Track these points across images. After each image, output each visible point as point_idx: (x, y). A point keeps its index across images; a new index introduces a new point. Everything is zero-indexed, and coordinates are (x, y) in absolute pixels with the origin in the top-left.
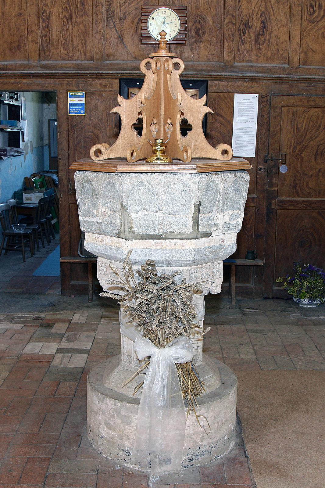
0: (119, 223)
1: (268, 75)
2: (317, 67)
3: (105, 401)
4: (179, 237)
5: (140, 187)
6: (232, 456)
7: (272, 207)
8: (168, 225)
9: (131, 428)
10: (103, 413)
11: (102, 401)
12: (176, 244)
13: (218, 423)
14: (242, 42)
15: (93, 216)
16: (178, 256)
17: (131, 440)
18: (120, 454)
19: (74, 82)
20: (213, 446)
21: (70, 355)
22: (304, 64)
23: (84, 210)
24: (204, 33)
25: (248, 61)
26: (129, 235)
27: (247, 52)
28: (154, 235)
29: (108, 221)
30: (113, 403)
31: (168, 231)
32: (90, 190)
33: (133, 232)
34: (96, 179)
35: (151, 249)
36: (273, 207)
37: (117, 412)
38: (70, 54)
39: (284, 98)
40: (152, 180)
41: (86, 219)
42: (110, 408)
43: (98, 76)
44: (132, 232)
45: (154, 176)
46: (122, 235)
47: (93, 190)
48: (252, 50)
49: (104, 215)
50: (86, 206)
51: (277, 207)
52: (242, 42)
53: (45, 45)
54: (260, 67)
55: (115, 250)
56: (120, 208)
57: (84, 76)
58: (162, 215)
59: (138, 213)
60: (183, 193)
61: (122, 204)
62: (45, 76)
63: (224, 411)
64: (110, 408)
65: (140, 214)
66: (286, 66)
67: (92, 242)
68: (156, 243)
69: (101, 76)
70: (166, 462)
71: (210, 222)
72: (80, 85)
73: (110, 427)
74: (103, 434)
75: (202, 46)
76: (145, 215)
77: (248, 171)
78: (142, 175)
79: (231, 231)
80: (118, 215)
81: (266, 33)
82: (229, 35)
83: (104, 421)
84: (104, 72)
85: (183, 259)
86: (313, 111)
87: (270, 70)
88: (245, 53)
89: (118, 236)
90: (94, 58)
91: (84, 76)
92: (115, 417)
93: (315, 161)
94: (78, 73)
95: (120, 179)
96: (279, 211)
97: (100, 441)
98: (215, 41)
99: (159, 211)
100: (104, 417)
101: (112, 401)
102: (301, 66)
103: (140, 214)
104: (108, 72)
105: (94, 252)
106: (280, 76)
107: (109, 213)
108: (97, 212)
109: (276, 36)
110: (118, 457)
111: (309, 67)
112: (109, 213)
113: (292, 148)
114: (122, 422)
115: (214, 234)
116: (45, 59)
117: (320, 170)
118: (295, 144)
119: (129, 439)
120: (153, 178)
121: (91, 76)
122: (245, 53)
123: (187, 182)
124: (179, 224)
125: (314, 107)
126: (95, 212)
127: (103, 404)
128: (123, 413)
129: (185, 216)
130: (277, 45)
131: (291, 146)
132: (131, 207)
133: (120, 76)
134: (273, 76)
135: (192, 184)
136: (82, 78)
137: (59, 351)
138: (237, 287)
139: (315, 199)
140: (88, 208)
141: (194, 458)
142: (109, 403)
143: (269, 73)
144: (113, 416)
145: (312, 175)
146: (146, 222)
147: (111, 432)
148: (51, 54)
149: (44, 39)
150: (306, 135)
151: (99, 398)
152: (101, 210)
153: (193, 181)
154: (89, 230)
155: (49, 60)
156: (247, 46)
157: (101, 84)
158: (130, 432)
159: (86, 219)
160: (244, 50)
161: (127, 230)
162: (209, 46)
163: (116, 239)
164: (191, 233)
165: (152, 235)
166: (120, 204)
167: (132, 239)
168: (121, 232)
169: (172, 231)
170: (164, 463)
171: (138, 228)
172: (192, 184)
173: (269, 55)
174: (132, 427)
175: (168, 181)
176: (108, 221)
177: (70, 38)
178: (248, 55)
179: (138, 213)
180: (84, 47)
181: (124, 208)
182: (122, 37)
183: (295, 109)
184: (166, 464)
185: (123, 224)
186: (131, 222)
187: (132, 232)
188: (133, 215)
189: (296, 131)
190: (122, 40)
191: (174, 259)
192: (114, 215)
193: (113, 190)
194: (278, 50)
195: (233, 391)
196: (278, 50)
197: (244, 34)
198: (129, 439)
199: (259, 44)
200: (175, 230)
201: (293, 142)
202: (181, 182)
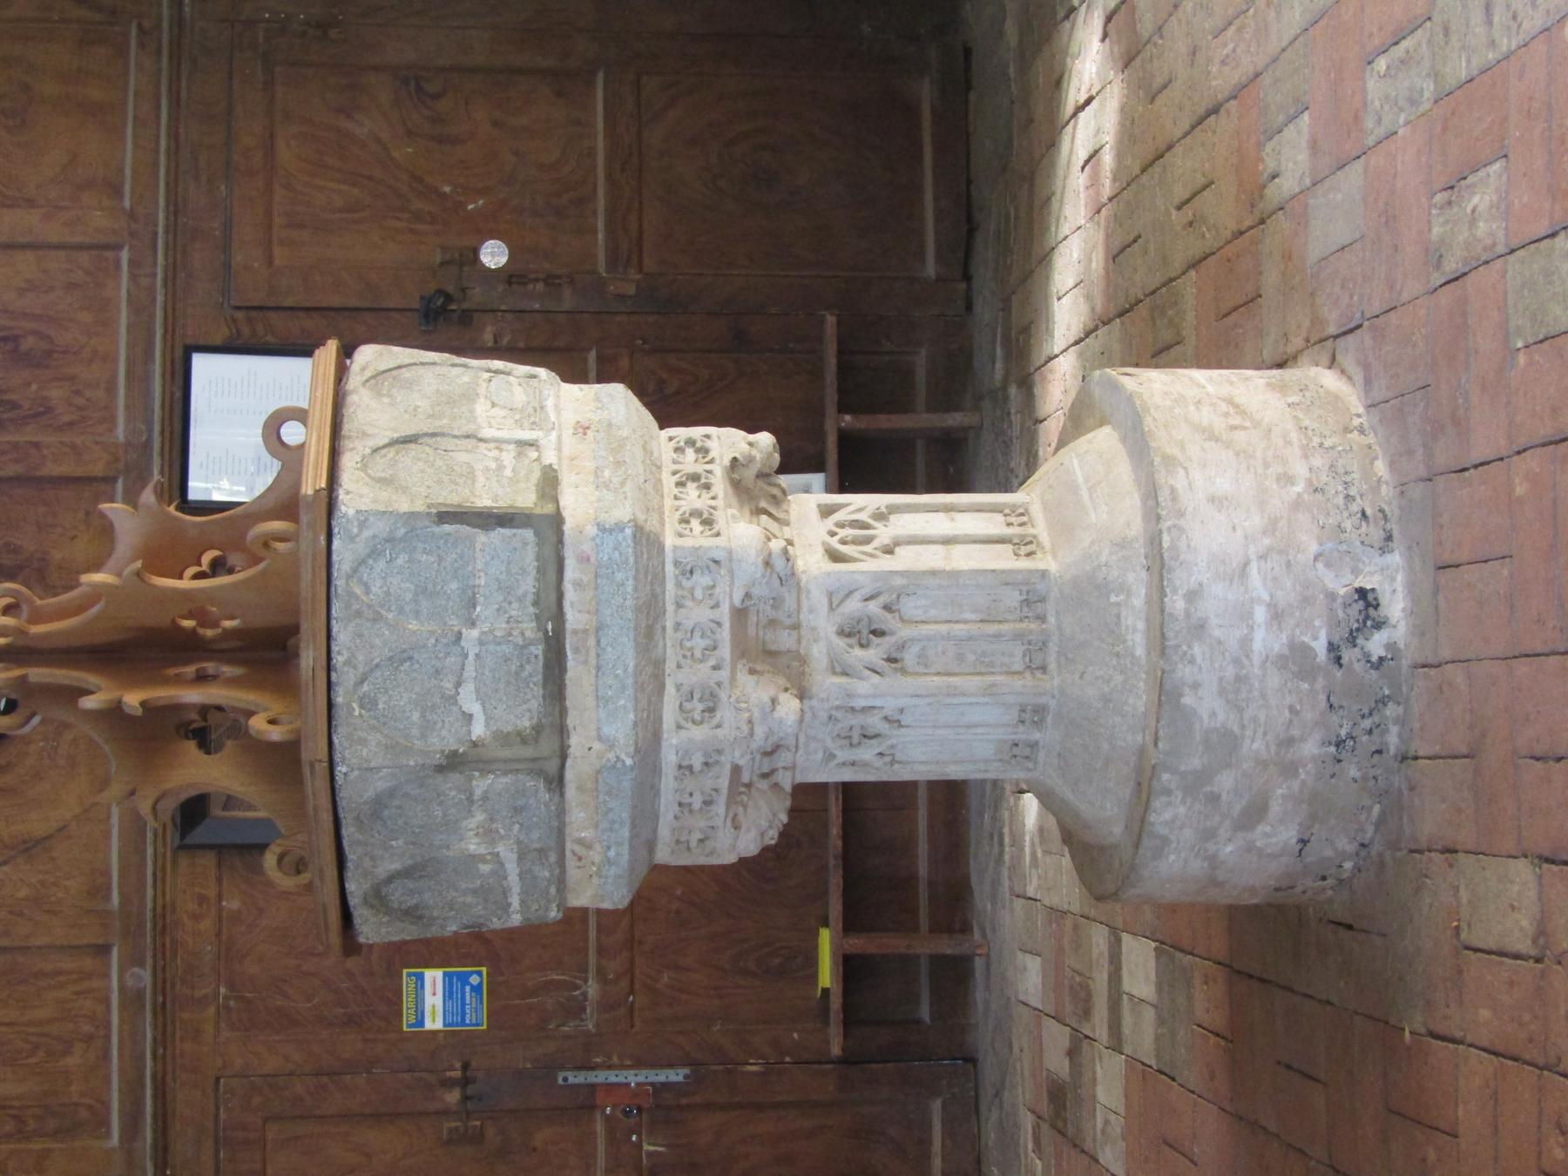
0: (505, 780)
1: (159, 314)
2: (130, 146)
3: (1163, 831)
4: (552, 576)
5: (381, 706)
6: (1359, 377)
7: (632, 290)
8: (514, 613)
9: (1248, 733)
10: (1209, 835)
11: (1165, 840)
12: (578, 585)
13: (1233, 428)
14: (42, 414)
15: (500, 873)
16: (619, 576)
17: (1295, 732)
18: (1353, 772)
19: (186, 1016)
20: (1316, 440)
21: (1125, 997)
22: (117, 192)
23: (485, 908)
24: (16, 550)
25: (111, 388)
26: (547, 746)
27: (78, 393)
28: (545, 658)
29: (507, 822)
30: (1164, 799)
31: (532, 610)
32: (410, 884)
33: (538, 729)
34: (367, 863)
35: (598, 668)
36: (631, 290)
37: (1195, 784)
38: (87, 1028)
39: (238, 259)
40: (355, 667)
41: (515, 901)
42: (1182, 810)
43: (164, 927)
44: (538, 733)
45: (339, 660)
46: (552, 767)
47: (406, 873)
48: (72, 378)
49: (488, 834)
50: (469, 899)
51: (633, 274)
52: (42, 414)
53: (52, 1124)
54: (131, 346)
55: (609, 793)
56: (455, 778)
57: (164, 982)
58: (475, 633)
59: (471, 716)
60: (400, 561)
61: (440, 769)
62: (164, 1122)
63: (1192, 408)
64: (1182, 810)
65: (475, 708)
66: (125, 255)
67: (595, 880)
68: (576, 650)
69: (164, 916)
70: (1368, 605)
71: (508, 472)
72: (198, 994)
73: (1255, 813)
74: (1288, 835)
75: (57, 555)
76: (477, 691)
77: (347, 352)
78: (339, 699)
79: (550, 403)
80: (481, 785)
81: (10, 328)
82: (17, 461)
83: (1240, 834)
84: (149, 905)
85: (632, 560)
86: (286, 154)
87: (141, 310)
88: (79, 401)
89: (557, 782)
90: (101, 941)
91: (164, 982)
92: (1215, 789)
93: (1470, 229)
94: (154, 1003)
95: (353, 776)
96: (649, 263)
97: (1320, 850)
98: (42, 509)
99: (463, 643)
100: (1223, 833)
101: (1157, 803)
102: (127, 204)
103: (475, 708)
104: (150, 892)
105: (632, 869)
106: (160, 276)
107: (480, 817)
108: (485, 862)
109: (21, 292)
110: (1365, 778)
111: (128, 172)
112: (480, 817)
113: (419, 227)
114: (1229, 766)
115: (550, 458)
116: (105, 1122)
117: (495, 124)
118: (406, 216)
119: (1290, 742)
120: (348, 662)
121: (164, 953)
122: (79, 401)
123: (361, 548)
124: (508, 572)
125: (270, 152)
126: (485, 868)
127: (1173, 838)
128: (1195, 763)
129: (478, 554)
130: (51, 289)
131: (412, 231)
132: (445, 739)
133: (164, 846)
134: (160, 299)
135: (367, 533)
136: (173, 986)
137: (1116, 1045)
138: (932, 408)
139: (600, 138)
140: (475, 892)
141: (1355, 507)
142: (1167, 816)
143: (152, 316)
144: (1214, 799)
145: (516, 153)
146: (502, 686)
147: (1275, 807)
148: (87, 1101)
149: (32, 1125)
150: (369, 178)
151: (1158, 854)
152: (473, 846)
153: (355, 530)
154: (553, 890)
155: (107, 1106)
156: (56, 394)
157: (196, 917)
158: (1265, 734)
159: (515, 901)
160: (70, 404)
161: (528, 752)
162: (59, 530)
163: (571, 791)
164: (537, 534)
165: (546, 666)
166: (439, 778)
167: (562, 731)
168: (540, 773)
169: (530, 598)
170: (1371, 611)
171: (523, 714)
172: (367, 533)
173: (86, 317)
174: (1243, 727)
175: (359, 614)
176: (507, 822)
177: (32, 1030)
178: (88, 393)
179: (471, 716)
180: (61, 978)
181: (453, 763)
182: (25, 842)
183: (278, 220)
184: (1376, 607)
185: (509, 766)
186: (503, 738)
187: (538, 733)
188: (479, 730)
189: (356, 216)
190: (38, 842)
191: (630, 589)
192: (485, 798)
193: (396, 802)
194: (71, 286)
195: (1125, 380)
196: (71, 286)
197: (15, 406)
198: (1290, 742)
199: (49, 353)
200: (528, 585)
201: (398, 224)
202: (362, 569)
